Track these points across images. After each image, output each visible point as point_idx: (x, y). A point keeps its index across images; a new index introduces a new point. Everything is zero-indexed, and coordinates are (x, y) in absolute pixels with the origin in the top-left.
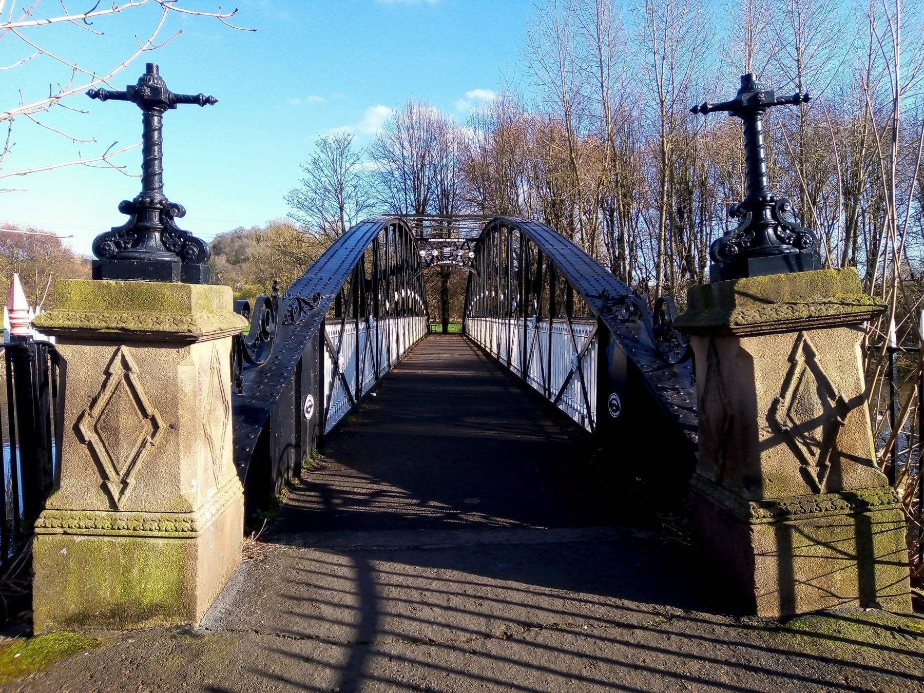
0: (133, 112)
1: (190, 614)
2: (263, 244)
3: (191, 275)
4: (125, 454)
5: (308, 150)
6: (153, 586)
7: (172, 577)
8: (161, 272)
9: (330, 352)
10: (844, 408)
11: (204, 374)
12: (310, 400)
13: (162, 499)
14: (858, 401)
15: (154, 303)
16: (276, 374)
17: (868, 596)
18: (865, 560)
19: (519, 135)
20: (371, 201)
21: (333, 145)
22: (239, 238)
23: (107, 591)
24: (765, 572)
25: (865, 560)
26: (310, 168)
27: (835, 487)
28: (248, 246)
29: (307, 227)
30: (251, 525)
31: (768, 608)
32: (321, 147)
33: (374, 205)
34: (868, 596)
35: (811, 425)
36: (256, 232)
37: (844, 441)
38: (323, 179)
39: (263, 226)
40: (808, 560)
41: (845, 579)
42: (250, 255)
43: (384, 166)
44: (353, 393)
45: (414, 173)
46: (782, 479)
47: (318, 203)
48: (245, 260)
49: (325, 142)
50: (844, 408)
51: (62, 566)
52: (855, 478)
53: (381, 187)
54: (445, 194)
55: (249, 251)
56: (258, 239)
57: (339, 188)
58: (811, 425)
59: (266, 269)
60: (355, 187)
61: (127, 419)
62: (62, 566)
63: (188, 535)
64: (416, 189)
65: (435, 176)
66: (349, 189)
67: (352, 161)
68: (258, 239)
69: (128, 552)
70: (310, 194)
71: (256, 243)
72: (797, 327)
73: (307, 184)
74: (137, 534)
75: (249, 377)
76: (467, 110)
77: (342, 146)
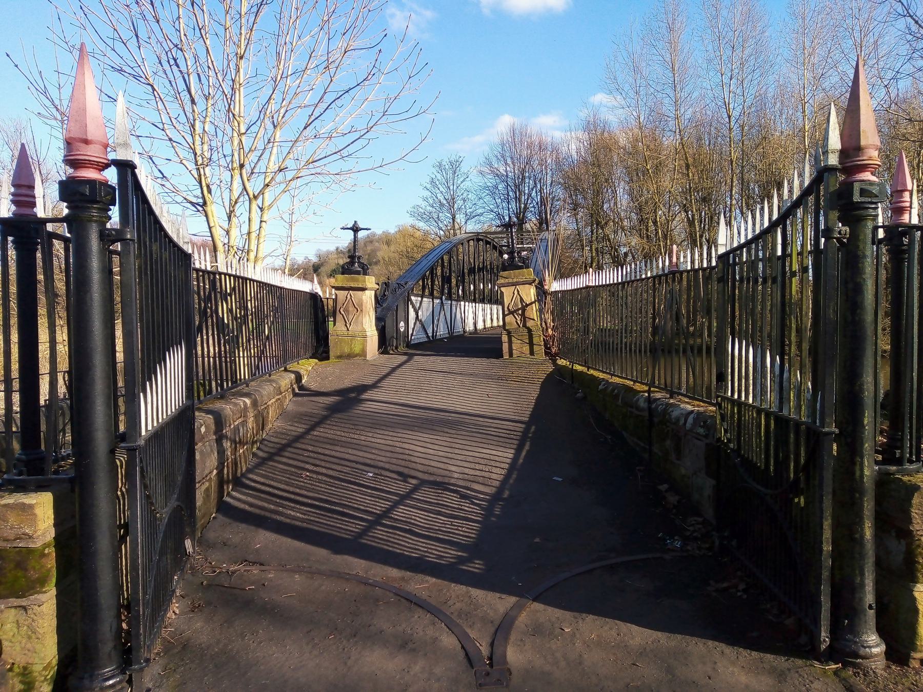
0: (351, 233)
1: (365, 356)
2: (392, 248)
3: (365, 274)
4: (351, 317)
5: (427, 172)
6: (357, 349)
7: (361, 347)
8: (358, 273)
9: (413, 307)
10: (527, 305)
11: (368, 298)
12: (402, 324)
13: (360, 328)
14: (531, 303)
15: (357, 280)
16: (388, 309)
17: (532, 353)
18: (531, 344)
19: (608, 149)
20: (480, 211)
21: (447, 167)
22: (371, 242)
23: (346, 350)
24: (505, 347)
25: (531, 344)
26: (429, 186)
27: (525, 325)
28: (379, 250)
29: (426, 233)
30: (380, 347)
31: (506, 356)
32: (437, 169)
33: (482, 214)
34: (532, 353)
35: (518, 310)
36: (386, 236)
37: (527, 314)
38: (439, 195)
39: (392, 230)
40: (516, 344)
41: (526, 349)
42: (380, 258)
43: (490, 181)
44: (430, 335)
45: (516, 186)
46: (510, 324)
47: (435, 216)
48: (376, 263)
49: (440, 165)
50: (527, 305)
51: (336, 343)
52: (530, 324)
53: (487, 198)
54: (543, 202)
55: (380, 254)
56: (388, 243)
57: (452, 201)
58: (518, 310)
59: (395, 271)
60: (464, 201)
61: (351, 309)
62: (336, 343)
63: (365, 337)
64: (517, 199)
65: (535, 186)
66: (459, 203)
67: (462, 179)
68: (388, 243)
69: (351, 340)
70: (429, 208)
71: (386, 247)
72: (514, 284)
73: (425, 199)
74: (354, 336)
75: (379, 310)
76: (559, 129)
77: (455, 166)
